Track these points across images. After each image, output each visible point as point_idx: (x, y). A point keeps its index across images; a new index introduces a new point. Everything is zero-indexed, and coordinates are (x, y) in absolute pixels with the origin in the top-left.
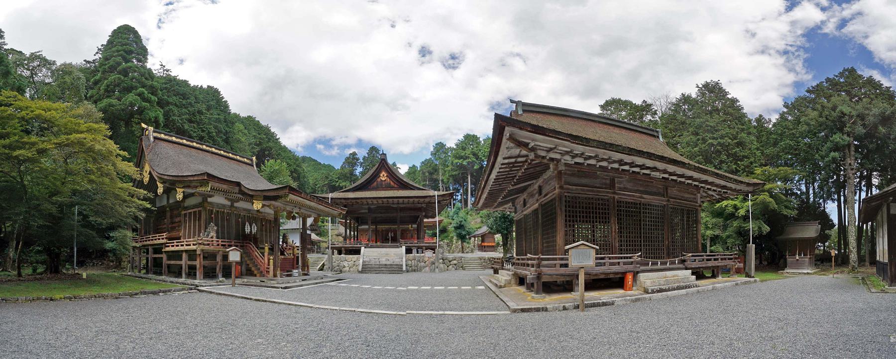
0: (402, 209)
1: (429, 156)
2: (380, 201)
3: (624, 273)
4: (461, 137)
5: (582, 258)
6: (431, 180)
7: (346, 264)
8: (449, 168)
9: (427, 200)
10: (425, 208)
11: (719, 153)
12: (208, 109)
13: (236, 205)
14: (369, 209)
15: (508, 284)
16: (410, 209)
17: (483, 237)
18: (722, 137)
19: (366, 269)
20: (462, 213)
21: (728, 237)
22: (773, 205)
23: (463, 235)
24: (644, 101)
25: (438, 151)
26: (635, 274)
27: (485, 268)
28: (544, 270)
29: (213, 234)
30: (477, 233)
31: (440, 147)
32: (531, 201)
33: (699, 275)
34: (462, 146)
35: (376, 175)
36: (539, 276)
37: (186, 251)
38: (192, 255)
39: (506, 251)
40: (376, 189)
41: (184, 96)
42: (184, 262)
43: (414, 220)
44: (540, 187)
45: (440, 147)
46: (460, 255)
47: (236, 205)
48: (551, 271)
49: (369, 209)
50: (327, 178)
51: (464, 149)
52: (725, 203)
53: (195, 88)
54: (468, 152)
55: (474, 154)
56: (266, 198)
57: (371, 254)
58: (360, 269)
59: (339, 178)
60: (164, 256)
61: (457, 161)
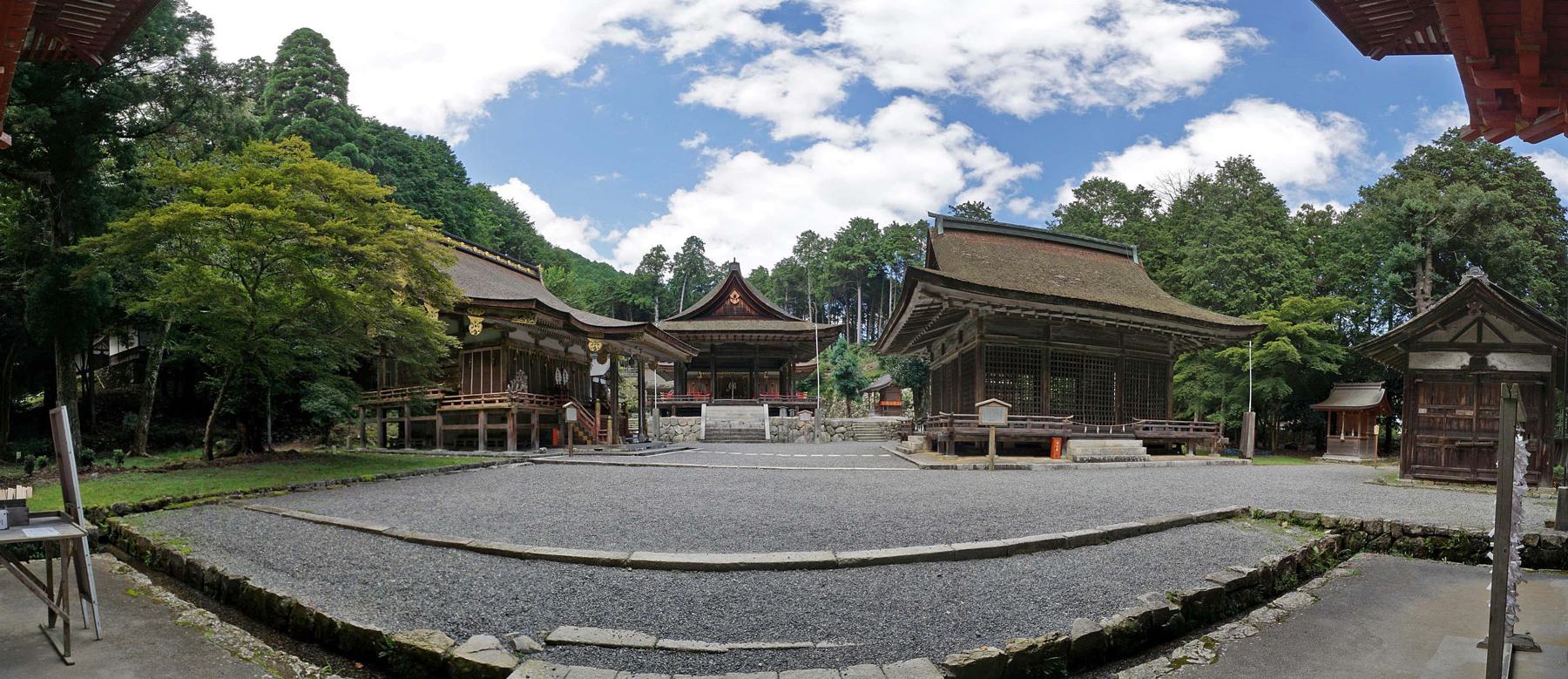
0: (763, 349)
1: (789, 254)
2: (731, 336)
3: (1050, 438)
4: (846, 224)
5: (993, 415)
6: (793, 294)
7: (678, 429)
8: (825, 276)
9: (802, 336)
10: (803, 345)
11: (1235, 274)
12: (440, 178)
13: (541, 343)
14: (712, 347)
15: (919, 449)
16: (775, 348)
17: (883, 391)
18: (1240, 250)
19: (712, 436)
20: (848, 355)
21: (1233, 401)
22: (1295, 354)
23: (850, 386)
24: (1141, 187)
25: (805, 246)
26: (1064, 440)
27: (885, 438)
28: (958, 429)
29: (524, 386)
30: (872, 385)
31: (809, 238)
32: (951, 347)
33: (1155, 447)
34: (846, 238)
35: (723, 295)
36: (951, 435)
37: (485, 410)
38: (498, 416)
39: (918, 413)
40: (724, 316)
41: (404, 156)
42: (482, 425)
43: (777, 364)
44: (961, 332)
45: (809, 238)
46: (845, 419)
47: (541, 343)
48: (963, 431)
49: (712, 347)
50: (611, 289)
51: (851, 244)
52: (1230, 351)
53: (418, 141)
54: (858, 249)
55: (868, 253)
56: (607, 337)
57: (715, 414)
58: (703, 436)
59: (633, 291)
61: (839, 264)
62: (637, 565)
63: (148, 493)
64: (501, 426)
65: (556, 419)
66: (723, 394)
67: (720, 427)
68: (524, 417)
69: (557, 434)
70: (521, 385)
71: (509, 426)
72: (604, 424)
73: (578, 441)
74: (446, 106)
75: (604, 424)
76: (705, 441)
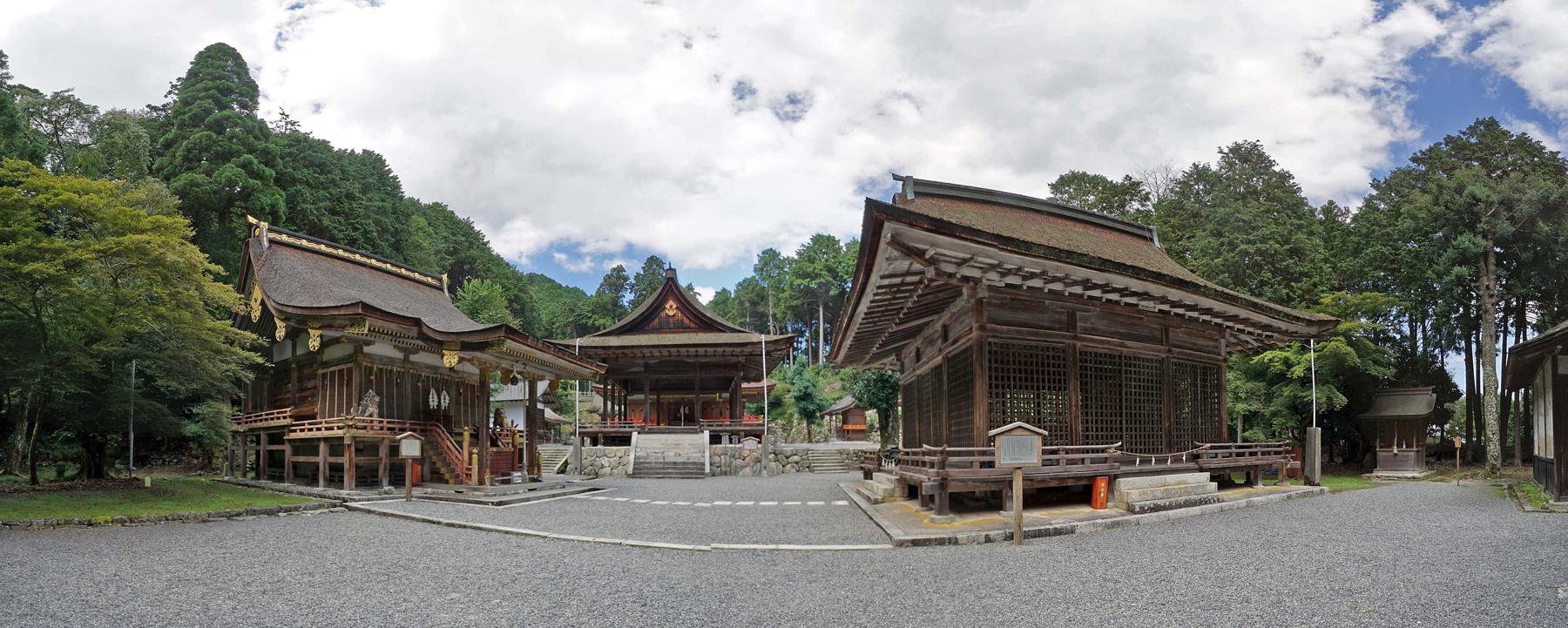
0: (703, 366)
1: (750, 274)
2: (665, 352)
3: (1093, 478)
4: (807, 240)
5: (1019, 451)
6: (754, 314)
7: (605, 461)
8: (786, 294)
9: (747, 350)
10: (744, 363)
11: (1258, 267)
12: (365, 190)
13: (413, 358)
14: (646, 365)
15: (889, 496)
16: (718, 366)
17: (846, 414)
18: (1264, 240)
19: (641, 470)
20: (808, 373)
21: (1274, 414)
22: (1353, 358)
23: (811, 411)
24: (1128, 177)
25: (766, 264)
26: (1112, 479)
27: (848, 468)
28: (953, 472)
29: (373, 409)
30: (834, 407)
31: (770, 258)
32: (929, 352)
33: (1223, 481)
34: (808, 255)
35: (657, 307)
36: (943, 483)
37: (326, 439)
38: (336, 445)
39: (886, 439)
40: (658, 330)
41: (322, 168)
42: (322, 458)
43: (725, 384)
44: (945, 328)
45: (770, 258)
46: (806, 445)
47: (413, 358)
48: (964, 475)
49: (646, 365)
50: (572, 311)
51: (812, 261)
52: (1268, 355)
53: (342, 154)
54: (819, 266)
55: (830, 270)
56: (466, 347)
57: (648, 444)
58: (630, 470)
59: (593, 312)
60: (287, 448)
61: (799, 281)
72: (471, 454)
75: (471, 454)
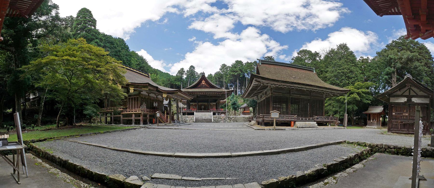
0: (211, 97)
1: (218, 70)
2: (202, 93)
3: (291, 121)
4: (234, 62)
5: (275, 115)
6: (219, 81)
7: (188, 119)
8: (228, 76)
9: (222, 93)
10: (222, 96)
11: (342, 76)
12: (122, 49)
13: (150, 95)
14: (197, 96)
15: (254, 124)
16: (215, 96)
17: (245, 108)
18: (343, 69)
19: (197, 121)
20: (235, 98)
21: (341, 111)
22: (358, 98)
23: (235, 107)
24: (316, 52)
25: (223, 68)
26: (295, 122)
27: (245, 121)
28: (265, 119)
29: (145, 107)
30: (241, 107)
31: (224, 66)
32: (263, 96)
33: (320, 124)
34: (234, 66)
35: (200, 82)
36: (263, 121)
37: (134, 114)
38: (138, 115)
39: (254, 114)
40: (200, 88)
41: (112, 43)
42: (133, 118)
43: (215, 101)
44: (266, 92)
45: (224, 66)
46: (234, 116)
47: (150, 95)
48: (267, 119)
49: (197, 96)
50: (169, 80)
51: (236, 68)
52: (340, 97)
53: (116, 39)
54: (237, 69)
55: (240, 70)
56: (168, 93)
57: (198, 115)
58: (194, 121)
59: (175, 80)
60: (121, 116)
61: (232, 73)
62: (176, 157)
63: (41, 137)
64: (139, 118)
65: (154, 116)
66: (200, 109)
67: (199, 118)
68: (145, 116)
69: (154, 120)
70: (144, 107)
71: (141, 118)
72: (167, 117)
73: (160, 122)
74: (123, 29)
75: (167, 117)
76: (195, 122)
